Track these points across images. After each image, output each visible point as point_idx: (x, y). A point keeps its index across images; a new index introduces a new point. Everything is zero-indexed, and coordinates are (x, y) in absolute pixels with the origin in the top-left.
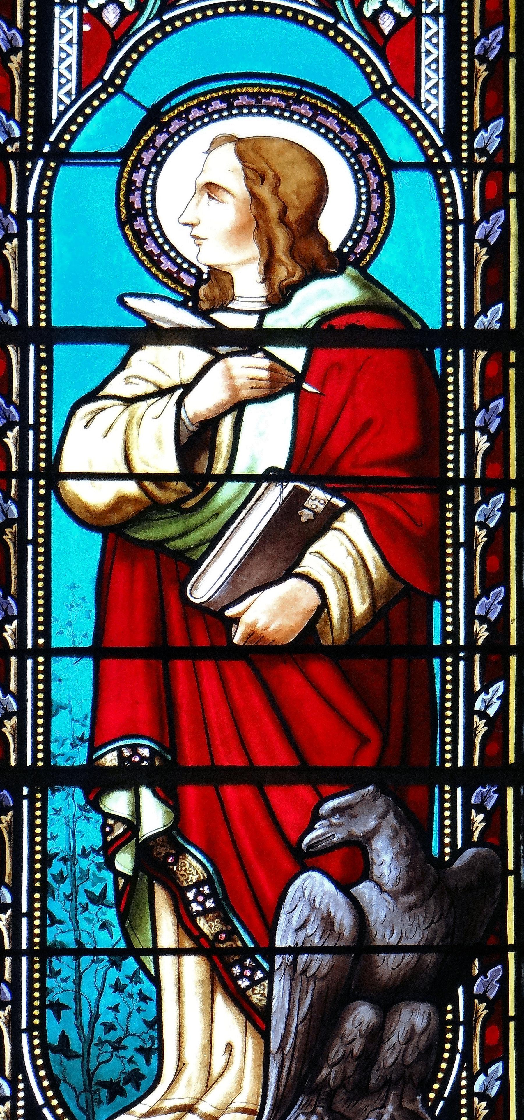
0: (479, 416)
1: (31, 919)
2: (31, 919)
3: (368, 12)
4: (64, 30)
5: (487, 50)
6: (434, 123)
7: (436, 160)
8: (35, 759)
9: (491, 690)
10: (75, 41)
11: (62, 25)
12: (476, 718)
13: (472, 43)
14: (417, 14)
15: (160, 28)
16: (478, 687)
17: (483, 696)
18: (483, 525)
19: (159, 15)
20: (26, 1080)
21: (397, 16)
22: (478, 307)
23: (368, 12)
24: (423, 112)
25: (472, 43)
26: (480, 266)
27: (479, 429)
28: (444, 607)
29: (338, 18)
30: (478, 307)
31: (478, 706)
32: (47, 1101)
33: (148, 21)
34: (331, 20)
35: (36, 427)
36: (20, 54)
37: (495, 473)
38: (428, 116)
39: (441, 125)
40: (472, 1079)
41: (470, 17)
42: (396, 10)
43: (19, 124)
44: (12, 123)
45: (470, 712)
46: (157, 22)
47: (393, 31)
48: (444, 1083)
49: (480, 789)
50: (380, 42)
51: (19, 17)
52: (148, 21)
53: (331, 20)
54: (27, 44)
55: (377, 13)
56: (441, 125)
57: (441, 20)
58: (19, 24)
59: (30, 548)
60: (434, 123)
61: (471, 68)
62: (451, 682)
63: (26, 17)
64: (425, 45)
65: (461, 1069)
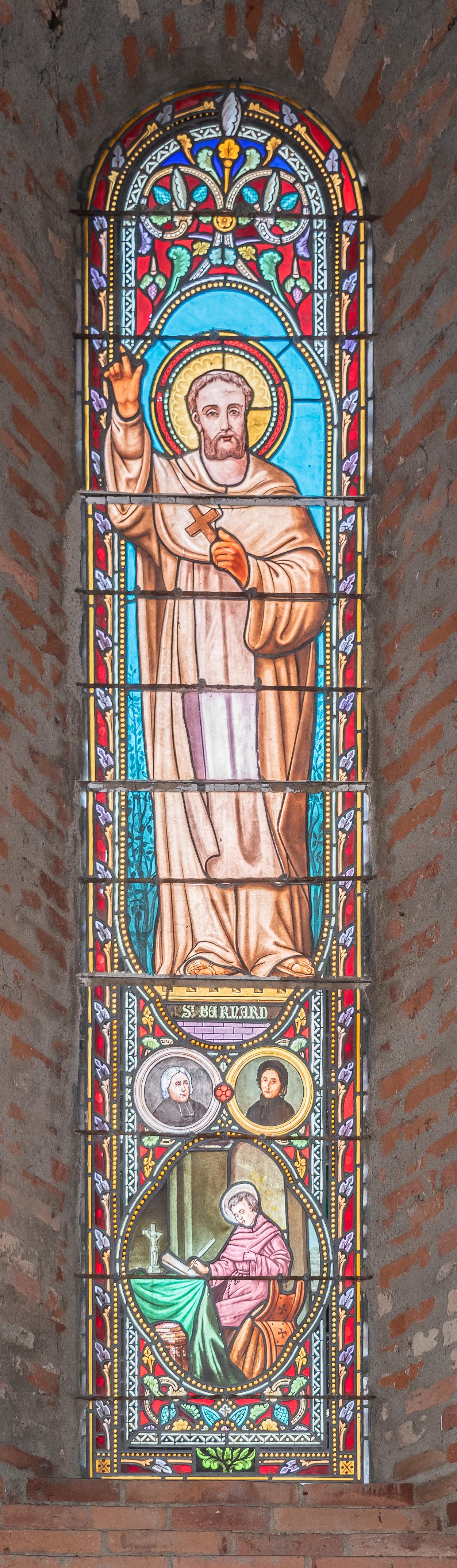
0: (342, 1016)
3: (289, 290)
6: (322, 360)
9: (351, 396)
10: (133, 310)
12: (339, 1253)
14: (312, 291)
15: (178, 298)
17: (347, 399)
19: (179, 288)
21: (303, 291)
22: (345, 455)
23: (289, 290)
24: (316, 352)
26: (342, 1378)
27: (344, 472)
28: (325, 638)
29: (273, 293)
30: (345, 455)
32: (128, 954)
33: (173, 293)
34: (269, 294)
36: (105, 292)
37: (349, 1274)
38: (318, 356)
39: (325, 361)
40: (338, 1296)
42: (302, 288)
43: (108, 1066)
44: (102, 399)
46: (178, 293)
47: (301, 301)
48: (323, 951)
49: (347, 280)
50: (294, 306)
51: (108, 1057)
52: (173, 293)
53: (269, 294)
54: (113, 1358)
56: (321, 1202)
60: (322, 360)
61: (336, 1201)
65: (332, 1290)
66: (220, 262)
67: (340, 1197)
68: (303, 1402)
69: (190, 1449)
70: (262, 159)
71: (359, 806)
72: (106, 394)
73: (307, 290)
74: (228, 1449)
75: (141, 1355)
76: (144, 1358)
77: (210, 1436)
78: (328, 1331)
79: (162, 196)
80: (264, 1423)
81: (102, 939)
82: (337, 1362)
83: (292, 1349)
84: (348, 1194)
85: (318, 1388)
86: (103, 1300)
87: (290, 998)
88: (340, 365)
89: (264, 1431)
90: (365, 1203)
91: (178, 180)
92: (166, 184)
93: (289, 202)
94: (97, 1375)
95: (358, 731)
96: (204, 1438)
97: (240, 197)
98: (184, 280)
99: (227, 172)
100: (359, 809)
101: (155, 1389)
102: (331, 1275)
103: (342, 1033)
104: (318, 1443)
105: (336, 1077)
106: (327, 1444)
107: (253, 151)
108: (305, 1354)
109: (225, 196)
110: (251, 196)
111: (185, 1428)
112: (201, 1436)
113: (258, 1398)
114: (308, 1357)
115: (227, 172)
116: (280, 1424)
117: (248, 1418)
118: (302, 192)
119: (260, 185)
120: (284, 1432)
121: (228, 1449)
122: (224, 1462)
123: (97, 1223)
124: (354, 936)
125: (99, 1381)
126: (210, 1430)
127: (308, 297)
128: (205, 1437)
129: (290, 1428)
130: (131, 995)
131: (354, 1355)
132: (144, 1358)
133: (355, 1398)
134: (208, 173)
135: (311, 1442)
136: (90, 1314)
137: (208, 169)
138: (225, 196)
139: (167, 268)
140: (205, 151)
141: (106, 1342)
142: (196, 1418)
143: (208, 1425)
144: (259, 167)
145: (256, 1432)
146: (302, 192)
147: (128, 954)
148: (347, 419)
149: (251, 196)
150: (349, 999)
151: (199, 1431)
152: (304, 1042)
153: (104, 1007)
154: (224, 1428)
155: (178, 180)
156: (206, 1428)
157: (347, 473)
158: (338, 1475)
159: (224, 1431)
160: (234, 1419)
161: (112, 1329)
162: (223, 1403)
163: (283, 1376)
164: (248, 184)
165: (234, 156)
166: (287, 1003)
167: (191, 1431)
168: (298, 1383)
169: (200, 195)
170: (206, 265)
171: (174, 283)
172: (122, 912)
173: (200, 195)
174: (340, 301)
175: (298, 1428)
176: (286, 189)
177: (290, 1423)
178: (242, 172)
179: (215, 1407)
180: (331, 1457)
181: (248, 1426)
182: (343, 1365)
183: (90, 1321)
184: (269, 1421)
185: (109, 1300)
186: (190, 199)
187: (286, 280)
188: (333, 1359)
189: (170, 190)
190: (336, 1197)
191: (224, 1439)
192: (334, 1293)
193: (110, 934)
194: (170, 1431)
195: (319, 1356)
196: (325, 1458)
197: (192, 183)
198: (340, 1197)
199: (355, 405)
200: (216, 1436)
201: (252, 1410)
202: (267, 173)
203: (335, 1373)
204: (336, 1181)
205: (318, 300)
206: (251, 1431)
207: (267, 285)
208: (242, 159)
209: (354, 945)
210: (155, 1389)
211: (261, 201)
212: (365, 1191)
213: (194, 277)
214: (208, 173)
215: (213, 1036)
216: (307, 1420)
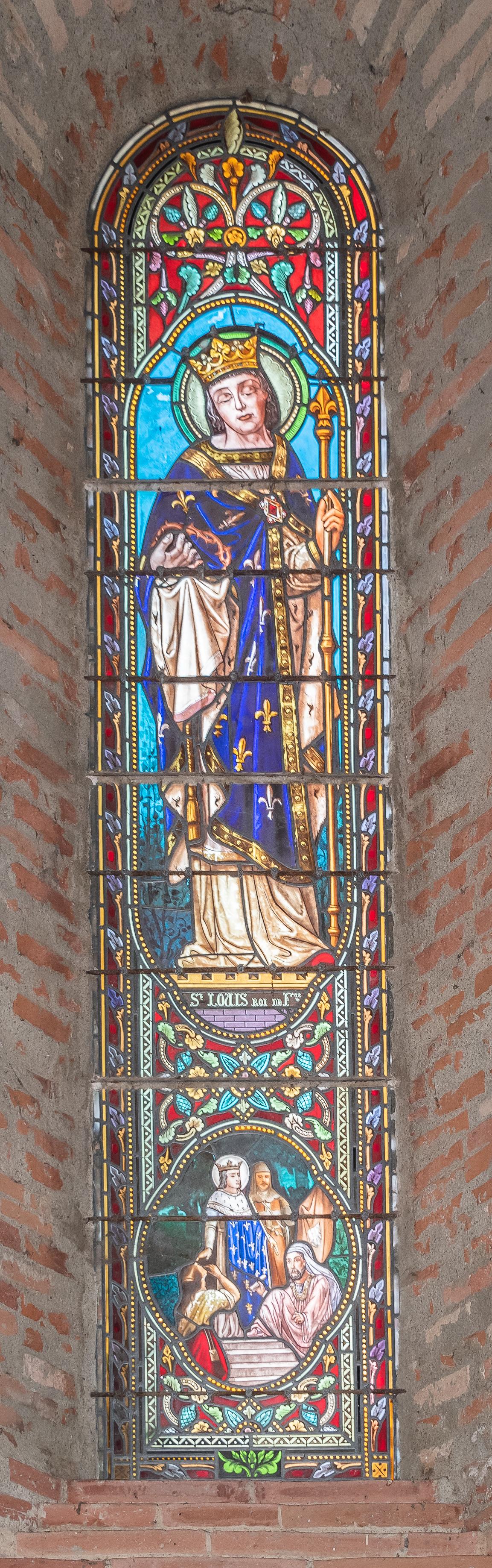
1: (132, 840)
2: (132, 840)
4: (147, 1134)
5: (364, 530)
6: (334, 363)
7: (339, 952)
8: (129, 566)
11: (144, 1099)
12: (359, 654)
13: (354, 288)
14: (324, 302)
16: (358, 520)
17: (360, 405)
18: (361, 415)
20: (130, 933)
23: (300, 301)
25: (354, 288)
31: (360, 588)
35: (129, 545)
36: (116, 360)
40: (367, 1290)
41: (352, 273)
45: (356, 650)
55: (303, 300)
57: (337, 307)
58: (116, 397)
59: (128, 841)
62: (345, 742)
63: (119, 335)
64: (328, 322)
66: (234, 280)
67: (366, 1067)
68: (331, 1398)
69: (212, 1452)
70: (267, 173)
71: (376, 392)
72: (117, 520)
73: (319, 299)
74: (252, 1452)
75: (160, 1354)
76: (164, 1358)
77: (232, 1438)
78: (359, 1430)
79: (173, 215)
80: (291, 1424)
81: (108, 356)
82: (364, 1125)
83: (313, 994)
84: (364, 298)
85: (348, 1383)
86: (118, 1122)
87: (311, 984)
88: (366, 1314)
89: (291, 1432)
90: (387, 722)
91: (189, 197)
92: (176, 202)
93: (298, 211)
94: (114, 1317)
95: (374, 319)
96: (229, 1441)
97: (249, 209)
98: (196, 298)
99: (233, 190)
100: (376, 396)
101: (171, 1035)
102: (361, 1253)
103: (368, 1016)
104: (349, 1444)
105: (353, 294)
106: (358, 1447)
107: (258, 167)
108: (327, 999)
109: (234, 213)
110: (259, 212)
111: (205, 1429)
112: (222, 1438)
113: (279, 1045)
114: (331, 1001)
115: (233, 190)
116: (307, 1424)
117: (269, 1065)
118: (311, 203)
119: (265, 200)
120: (312, 1433)
121: (252, 1452)
122: (247, 1465)
123: (111, 1040)
124: (379, 940)
125: (111, 857)
126: (232, 1433)
127: (320, 306)
128: (227, 1440)
129: (318, 1429)
130: (145, 975)
131: (370, 290)
132: (164, 1358)
133: (374, 572)
134: (213, 188)
135: (341, 1443)
136: (99, 555)
137: (211, 183)
138: (234, 213)
139: (179, 286)
140: (207, 166)
141: (112, 278)
142: (218, 1421)
143: (227, 1073)
144: (266, 181)
145: (282, 1433)
146: (311, 203)
147: (142, 948)
148: (371, 1249)
149: (259, 212)
150: (376, 1097)
151: (220, 1433)
152: (331, 1380)
153: (114, 522)
154: (247, 1430)
155: (189, 197)
156: (229, 1430)
157: (363, 652)
158: (372, 1460)
159: (248, 1433)
160: (256, 1095)
161: (119, 324)
162: (242, 1050)
163: (306, 1021)
164: (254, 200)
165: (240, 173)
166: (307, 989)
167: (214, 1433)
168: (327, 1381)
169: (211, 214)
170: (218, 285)
171: (185, 299)
172: (136, 906)
173: (211, 214)
174: (353, 308)
175: (327, 1429)
176: (293, 199)
177: (318, 1423)
178: (250, 187)
179: (235, 1054)
180: (362, 1459)
181: (271, 1074)
182: (369, 1129)
183: (106, 1197)
184: (296, 1422)
185: (123, 1121)
186: (201, 216)
187: (297, 291)
188: (360, 1122)
189: (180, 209)
190: (363, 1068)
191: (247, 1441)
192: (358, 939)
193: (120, 884)
194: (189, 1433)
195: (343, 1127)
196: (357, 1460)
197: (203, 202)
198: (366, 1067)
199: (380, 1235)
200: (239, 1438)
201: (274, 1058)
202: (275, 184)
203: (360, 1028)
204: (363, 1110)
205: (330, 311)
206: (276, 1432)
207: (278, 297)
208: (248, 176)
209: (378, 950)
210: (171, 1035)
211: (270, 214)
212: (396, 1281)
213: (202, 297)
214: (213, 188)
215: (232, 1024)
216: (336, 1421)
